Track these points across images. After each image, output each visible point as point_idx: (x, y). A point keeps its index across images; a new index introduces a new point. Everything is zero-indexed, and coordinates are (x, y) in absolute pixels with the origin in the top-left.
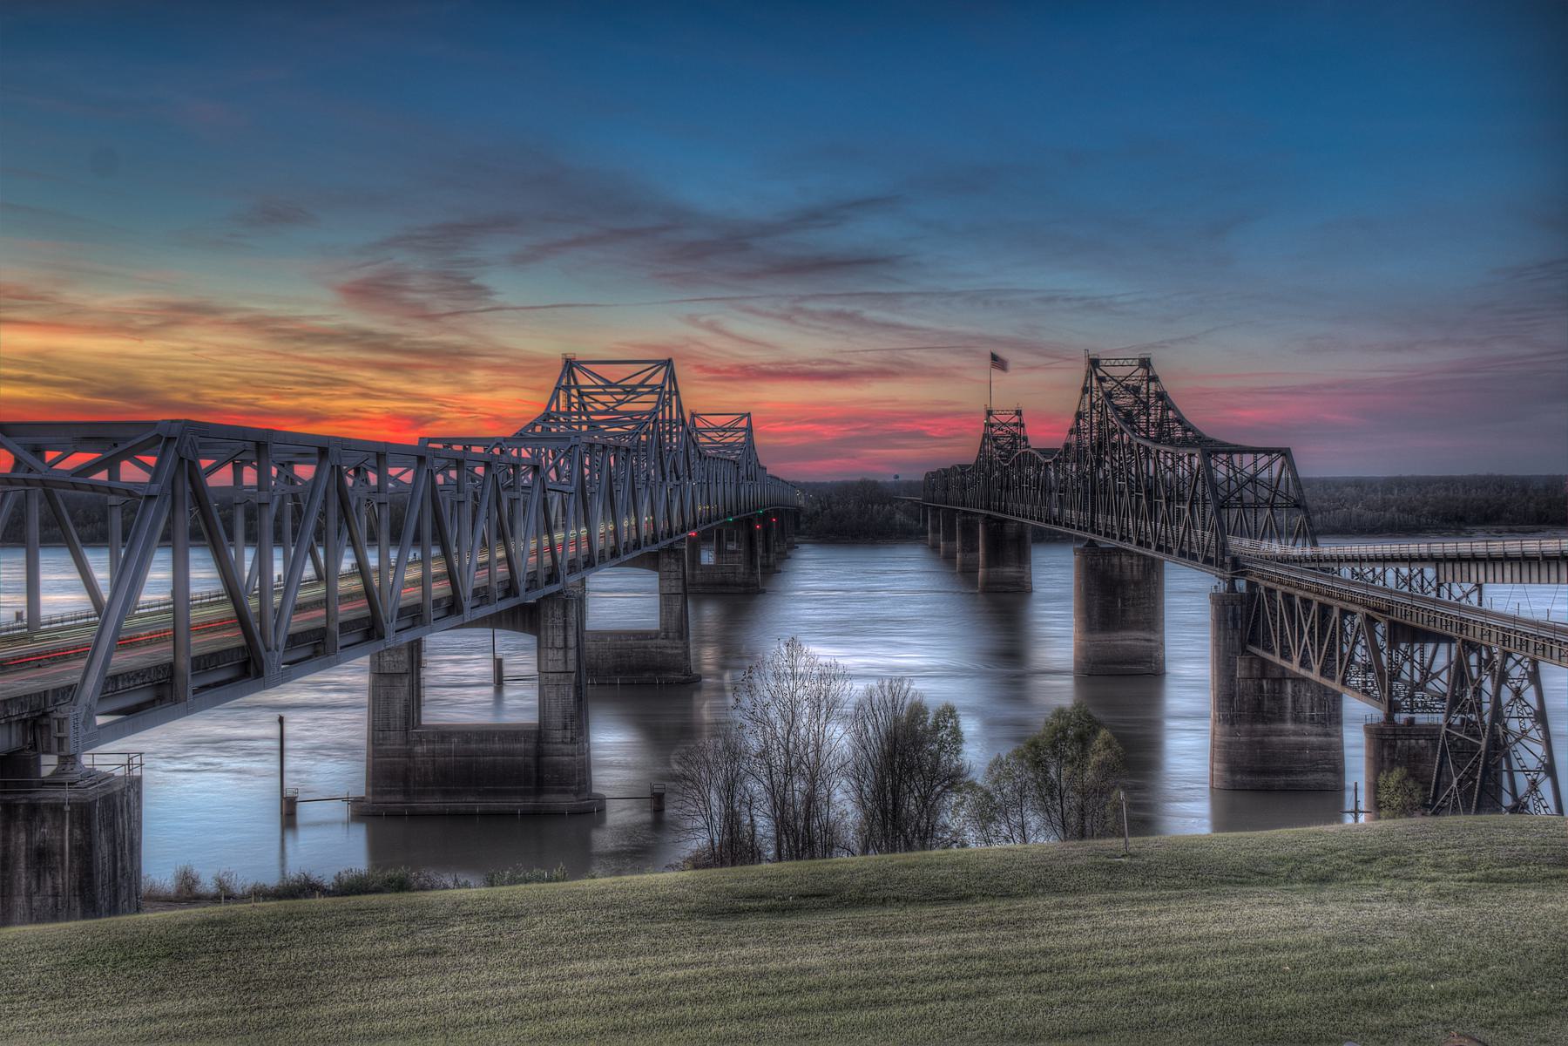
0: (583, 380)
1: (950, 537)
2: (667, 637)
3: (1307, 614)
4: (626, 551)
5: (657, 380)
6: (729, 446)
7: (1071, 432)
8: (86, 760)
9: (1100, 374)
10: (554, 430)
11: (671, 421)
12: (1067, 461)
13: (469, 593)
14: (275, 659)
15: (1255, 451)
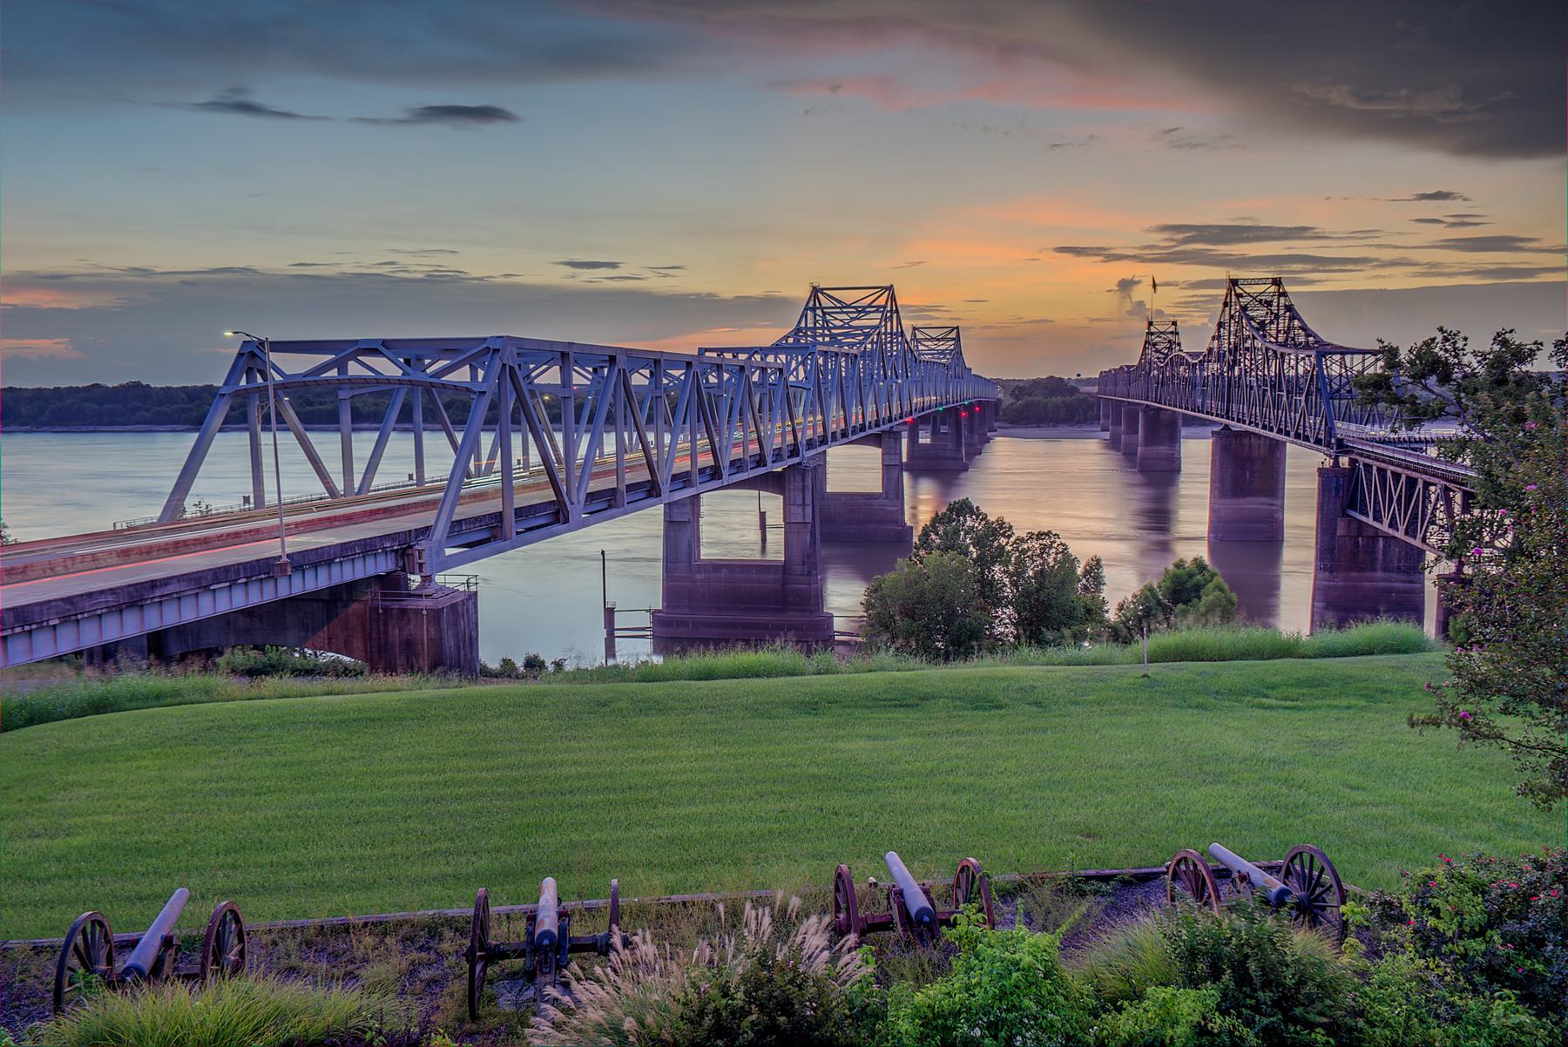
0: (825, 302)
1: (1117, 422)
2: (887, 498)
3: (1396, 486)
4: (854, 433)
5: (881, 301)
6: (942, 352)
7: (1213, 338)
8: (439, 579)
9: (1239, 291)
10: (802, 341)
11: (891, 333)
12: (1209, 361)
13: (727, 464)
14: (576, 510)
15: (1363, 352)
